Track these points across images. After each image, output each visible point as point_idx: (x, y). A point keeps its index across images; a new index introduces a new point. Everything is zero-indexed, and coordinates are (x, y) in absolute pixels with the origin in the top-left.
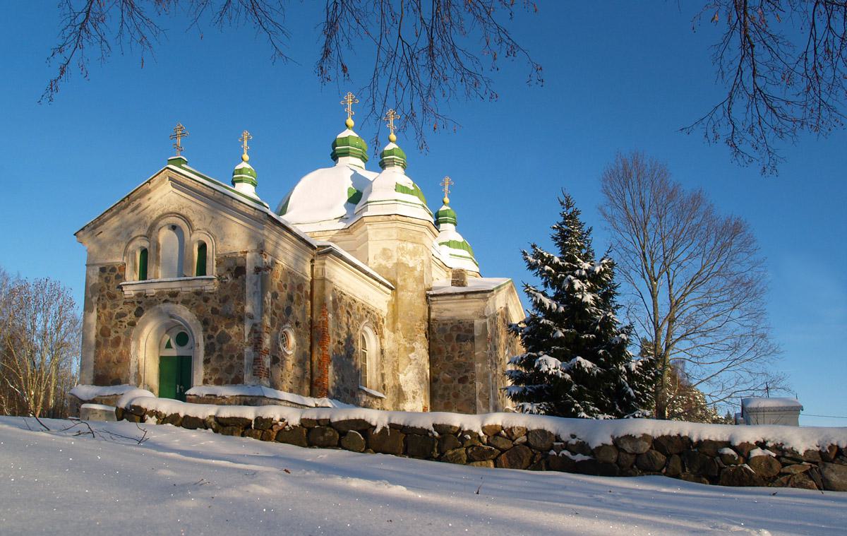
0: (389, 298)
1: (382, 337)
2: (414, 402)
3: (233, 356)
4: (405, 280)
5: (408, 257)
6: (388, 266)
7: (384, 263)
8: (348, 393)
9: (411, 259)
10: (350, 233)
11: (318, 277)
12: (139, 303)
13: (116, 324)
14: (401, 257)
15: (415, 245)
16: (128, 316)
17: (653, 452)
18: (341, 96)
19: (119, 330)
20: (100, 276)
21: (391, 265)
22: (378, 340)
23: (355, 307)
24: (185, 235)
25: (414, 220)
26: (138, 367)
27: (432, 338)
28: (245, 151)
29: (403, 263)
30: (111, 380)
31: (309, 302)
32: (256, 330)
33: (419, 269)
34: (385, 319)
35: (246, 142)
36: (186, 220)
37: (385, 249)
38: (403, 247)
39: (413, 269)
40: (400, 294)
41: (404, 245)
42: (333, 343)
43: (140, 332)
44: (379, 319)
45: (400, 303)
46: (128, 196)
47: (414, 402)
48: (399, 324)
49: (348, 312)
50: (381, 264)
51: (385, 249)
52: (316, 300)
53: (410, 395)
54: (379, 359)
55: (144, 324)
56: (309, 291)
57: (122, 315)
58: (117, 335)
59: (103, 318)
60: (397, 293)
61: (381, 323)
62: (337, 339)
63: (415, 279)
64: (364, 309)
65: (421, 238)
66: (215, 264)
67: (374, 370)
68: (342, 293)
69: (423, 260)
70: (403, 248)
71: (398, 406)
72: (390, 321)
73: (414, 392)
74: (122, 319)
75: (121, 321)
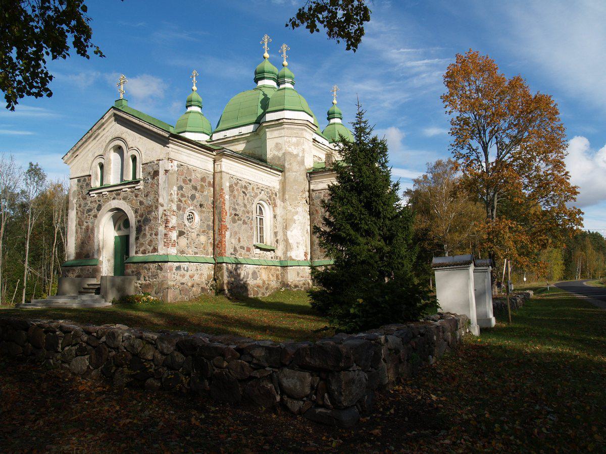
0: (280, 178)
1: (275, 205)
2: (298, 250)
3: (152, 234)
4: (290, 164)
5: (293, 147)
6: (279, 155)
7: (276, 153)
8: (244, 249)
9: (295, 149)
10: (257, 134)
11: (218, 171)
12: (99, 201)
13: (87, 217)
14: (288, 148)
15: (298, 139)
16: (93, 211)
17: (176, 353)
18: (261, 38)
19: (88, 221)
20: (78, 185)
21: (281, 154)
22: (272, 209)
23: (250, 188)
24: (124, 152)
25: (296, 121)
26: (99, 246)
27: (311, 203)
28: (194, 84)
29: (289, 152)
30: (84, 255)
31: (212, 189)
32: (165, 214)
33: (301, 155)
34: (278, 193)
35: (194, 78)
36: (118, 138)
37: (277, 144)
38: (289, 141)
39: (297, 155)
40: (287, 174)
41: (290, 139)
42: (230, 216)
43: (99, 222)
44: (272, 193)
45: (287, 180)
46: (91, 129)
47: (298, 250)
48: (286, 195)
49: (244, 192)
50: (274, 155)
51: (277, 144)
52: (217, 188)
53: (294, 246)
54: (272, 221)
55: (103, 215)
56: (212, 181)
57: (89, 210)
58: (259, 193)
59: (79, 213)
60: (285, 174)
61: (274, 196)
62: (233, 212)
63: (298, 162)
64: (258, 188)
65: (302, 133)
66: (141, 170)
67: (269, 230)
68: (238, 179)
69: (304, 149)
70: (289, 142)
71: (286, 254)
72: (281, 194)
73: (297, 243)
74: (90, 213)
75: (89, 215)
